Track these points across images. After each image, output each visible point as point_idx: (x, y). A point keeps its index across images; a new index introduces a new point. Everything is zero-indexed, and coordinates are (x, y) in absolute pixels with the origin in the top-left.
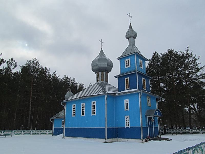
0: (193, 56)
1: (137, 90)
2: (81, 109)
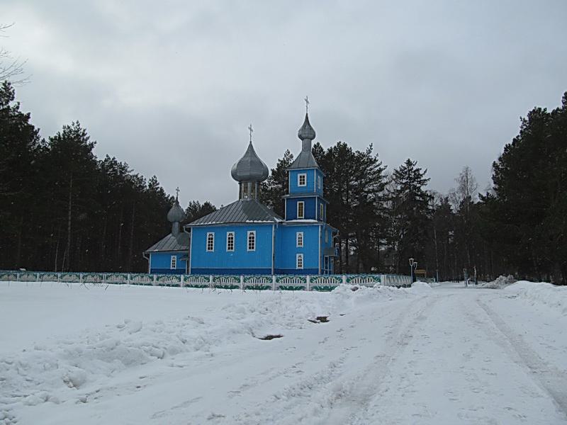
0: (377, 163)
1: (314, 221)
2: (246, 245)
